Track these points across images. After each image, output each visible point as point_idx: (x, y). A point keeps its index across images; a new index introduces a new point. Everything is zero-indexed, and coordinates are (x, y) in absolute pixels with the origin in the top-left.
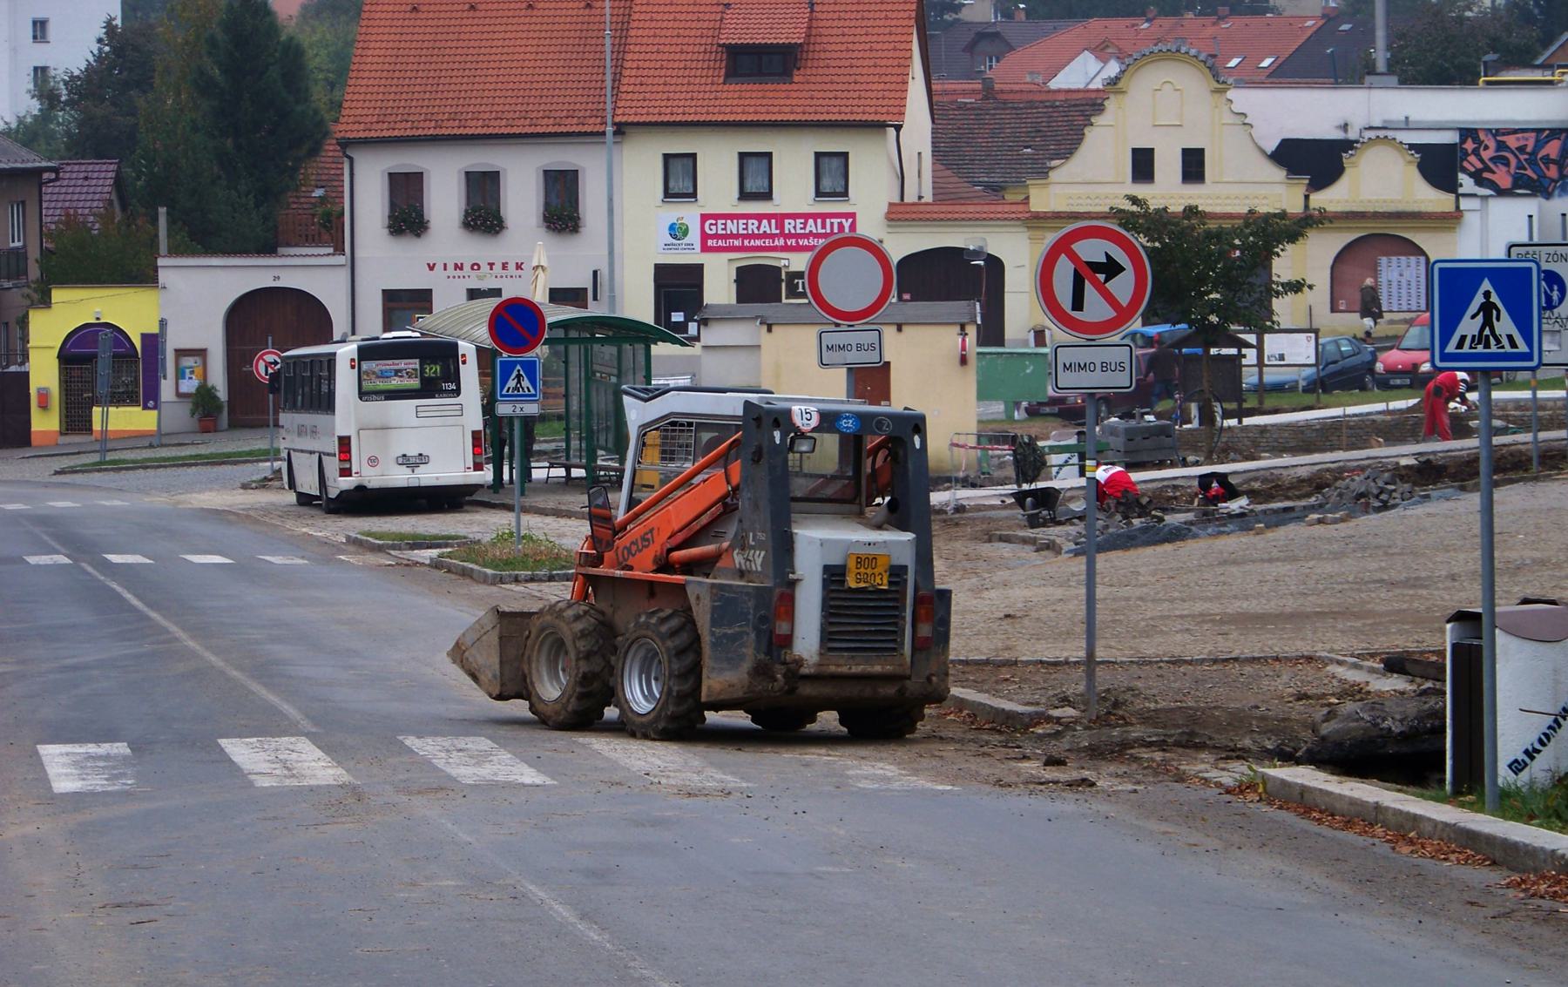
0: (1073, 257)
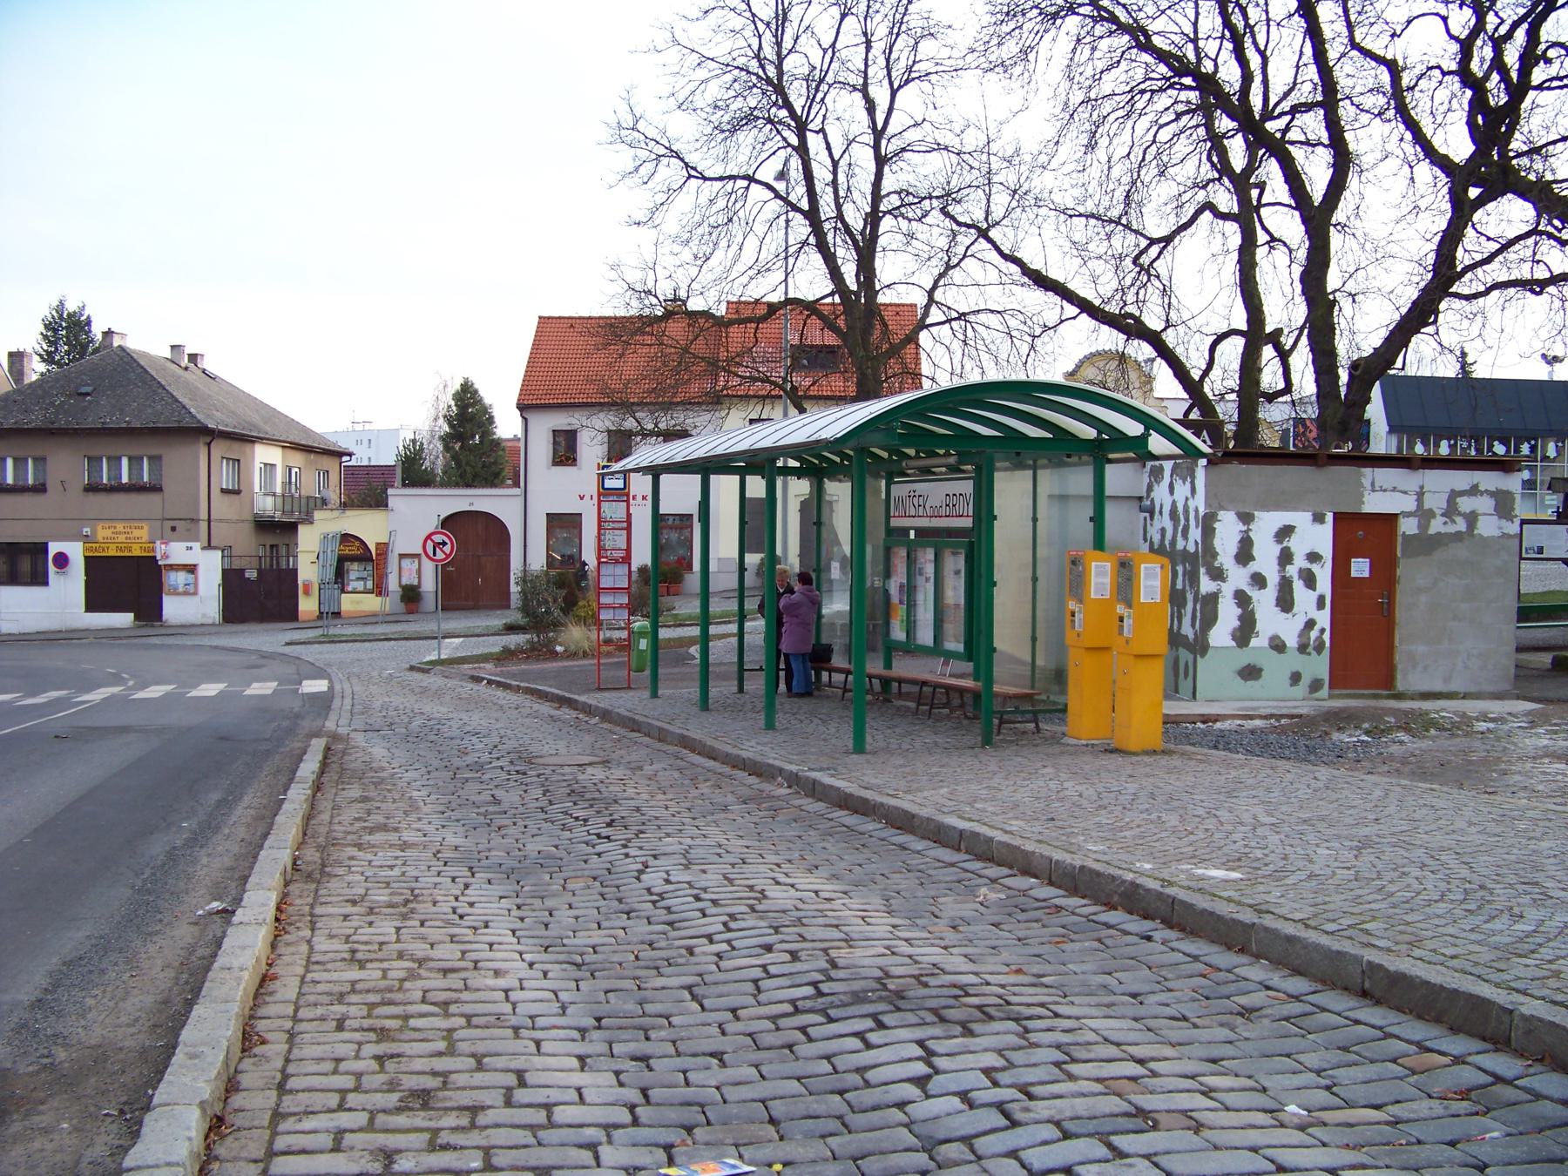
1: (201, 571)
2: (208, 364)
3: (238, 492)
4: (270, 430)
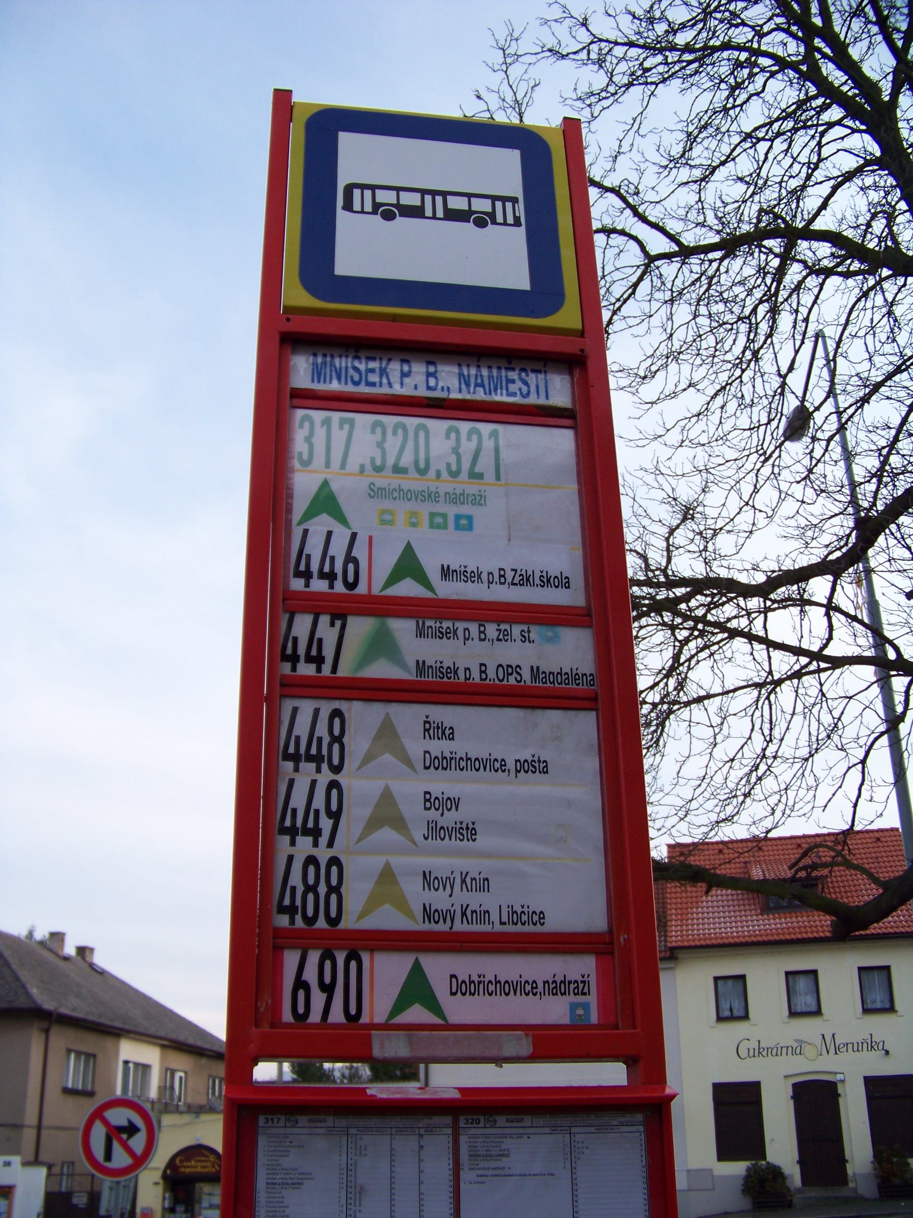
0: (106, 1122)
1: (19, 1196)
2: (100, 960)
4: (145, 1025)
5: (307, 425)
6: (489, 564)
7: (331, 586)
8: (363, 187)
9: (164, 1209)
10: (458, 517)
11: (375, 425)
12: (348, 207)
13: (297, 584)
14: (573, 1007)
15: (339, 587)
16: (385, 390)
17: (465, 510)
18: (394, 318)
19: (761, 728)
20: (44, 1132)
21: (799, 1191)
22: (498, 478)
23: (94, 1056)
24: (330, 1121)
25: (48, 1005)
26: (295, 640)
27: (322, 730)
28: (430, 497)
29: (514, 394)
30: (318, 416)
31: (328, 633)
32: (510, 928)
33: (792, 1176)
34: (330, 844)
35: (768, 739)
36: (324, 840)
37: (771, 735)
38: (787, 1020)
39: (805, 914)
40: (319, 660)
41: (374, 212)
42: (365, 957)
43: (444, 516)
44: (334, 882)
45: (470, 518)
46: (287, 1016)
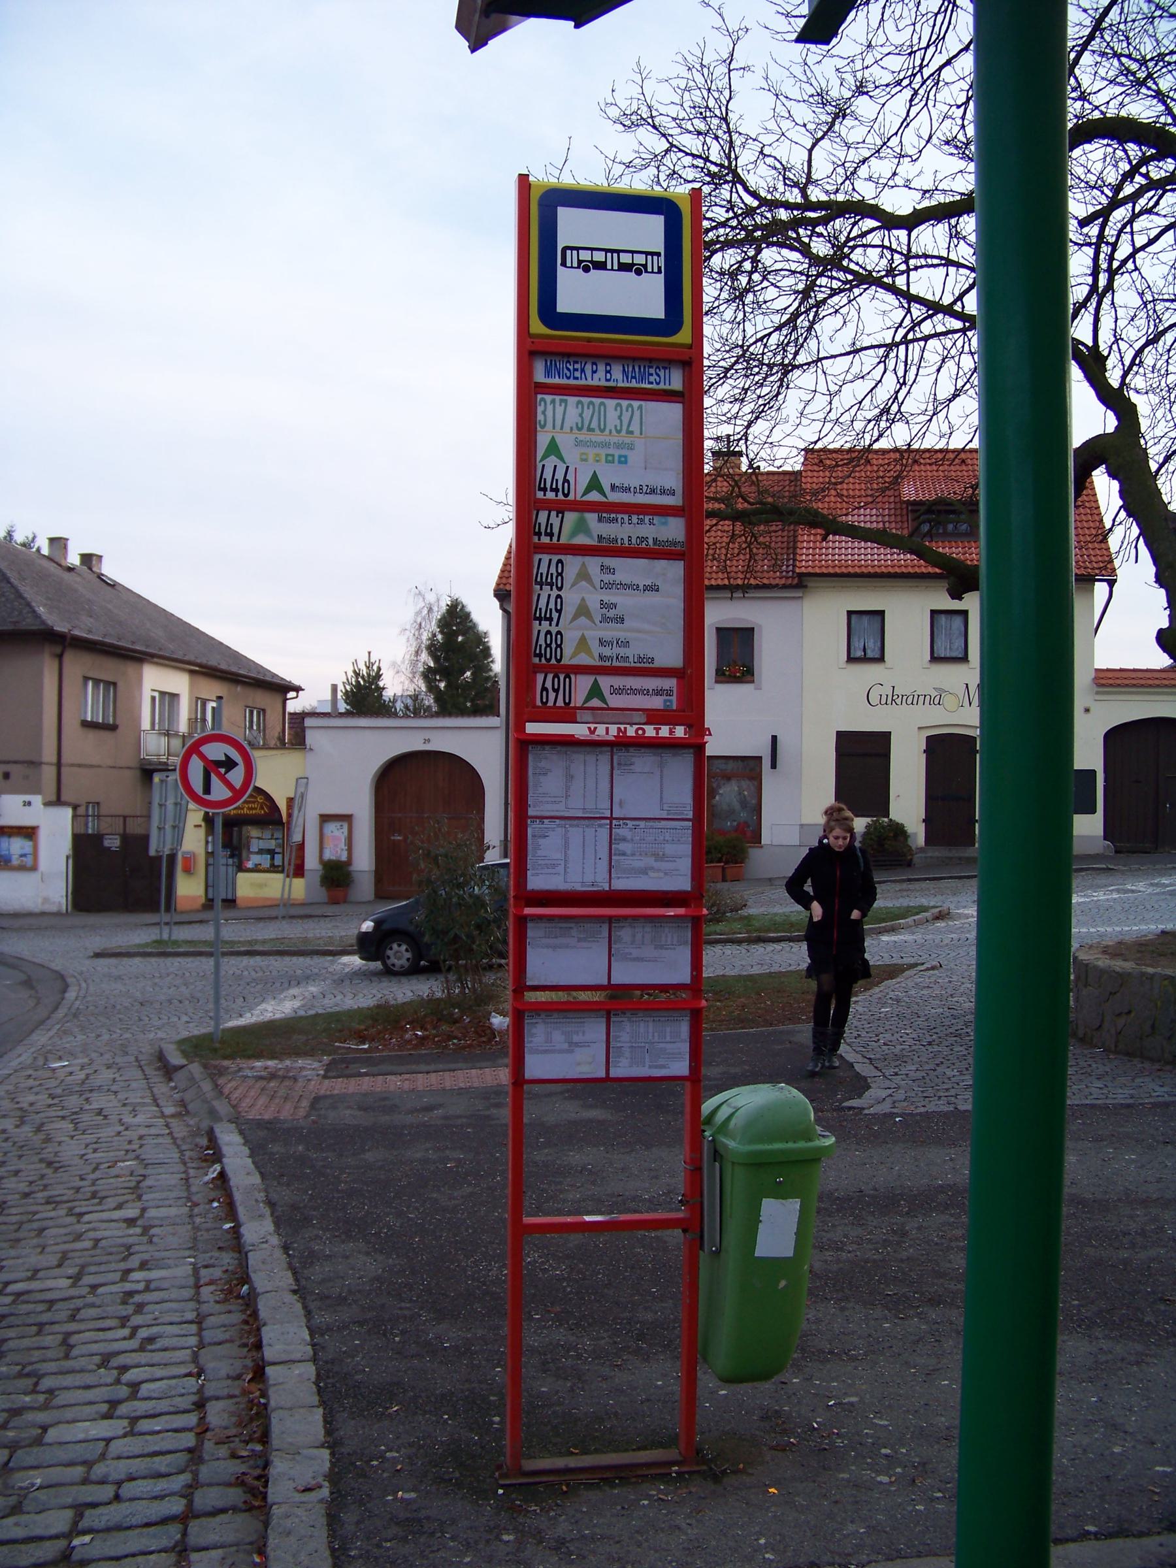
0: (203, 757)
1: (43, 836)
2: (108, 569)
3: (113, 728)
4: (171, 648)
5: (543, 403)
6: (634, 483)
7: (557, 496)
8: (572, 248)
9: (207, 853)
10: (620, 457)
11: (579, 402)
12: (564, 264)
13: (540, 495)
14: (665, 701)
15: (561, 496)
16: (582, 382)
17: (623, 452)
18: (589, 340)
19: (895, 370)
20: (64, 770)
21: (921, 850)
22: (641, 434)
23: (115, 684)
24: (559, 748)
25: (62, 627)
26: (540, 524)
27: (553, 570)
28: (606, 445)
29: (652, 383)
30: (548, 398)
31: (555, 520)
32: (638, 665)
33: (915, 834)
34: (557, 625)
35: (901, 381)
36: (554, 623)
37: (904, 377)
38: (928, 665)
39: (960, 544)
40: (551, 535)
41: (578, 267)
42: (573, 677)
43: (613, 456)
44: (559, 643)
45: (625, 457)
46: (539, 703)
